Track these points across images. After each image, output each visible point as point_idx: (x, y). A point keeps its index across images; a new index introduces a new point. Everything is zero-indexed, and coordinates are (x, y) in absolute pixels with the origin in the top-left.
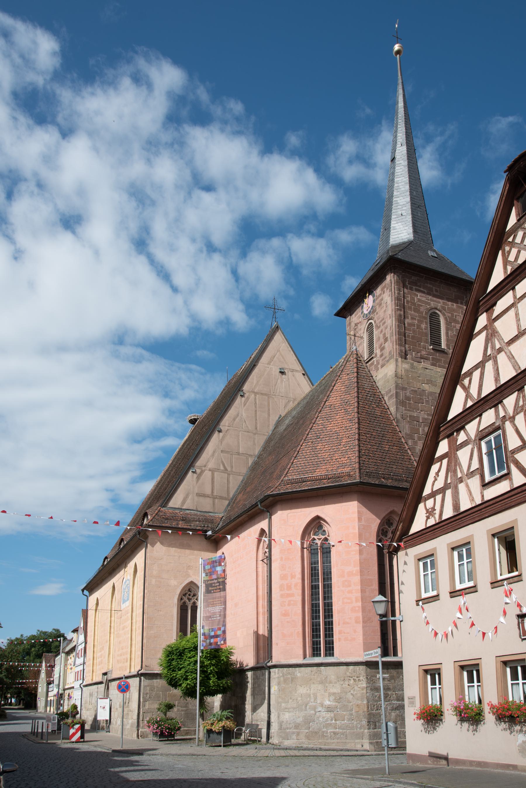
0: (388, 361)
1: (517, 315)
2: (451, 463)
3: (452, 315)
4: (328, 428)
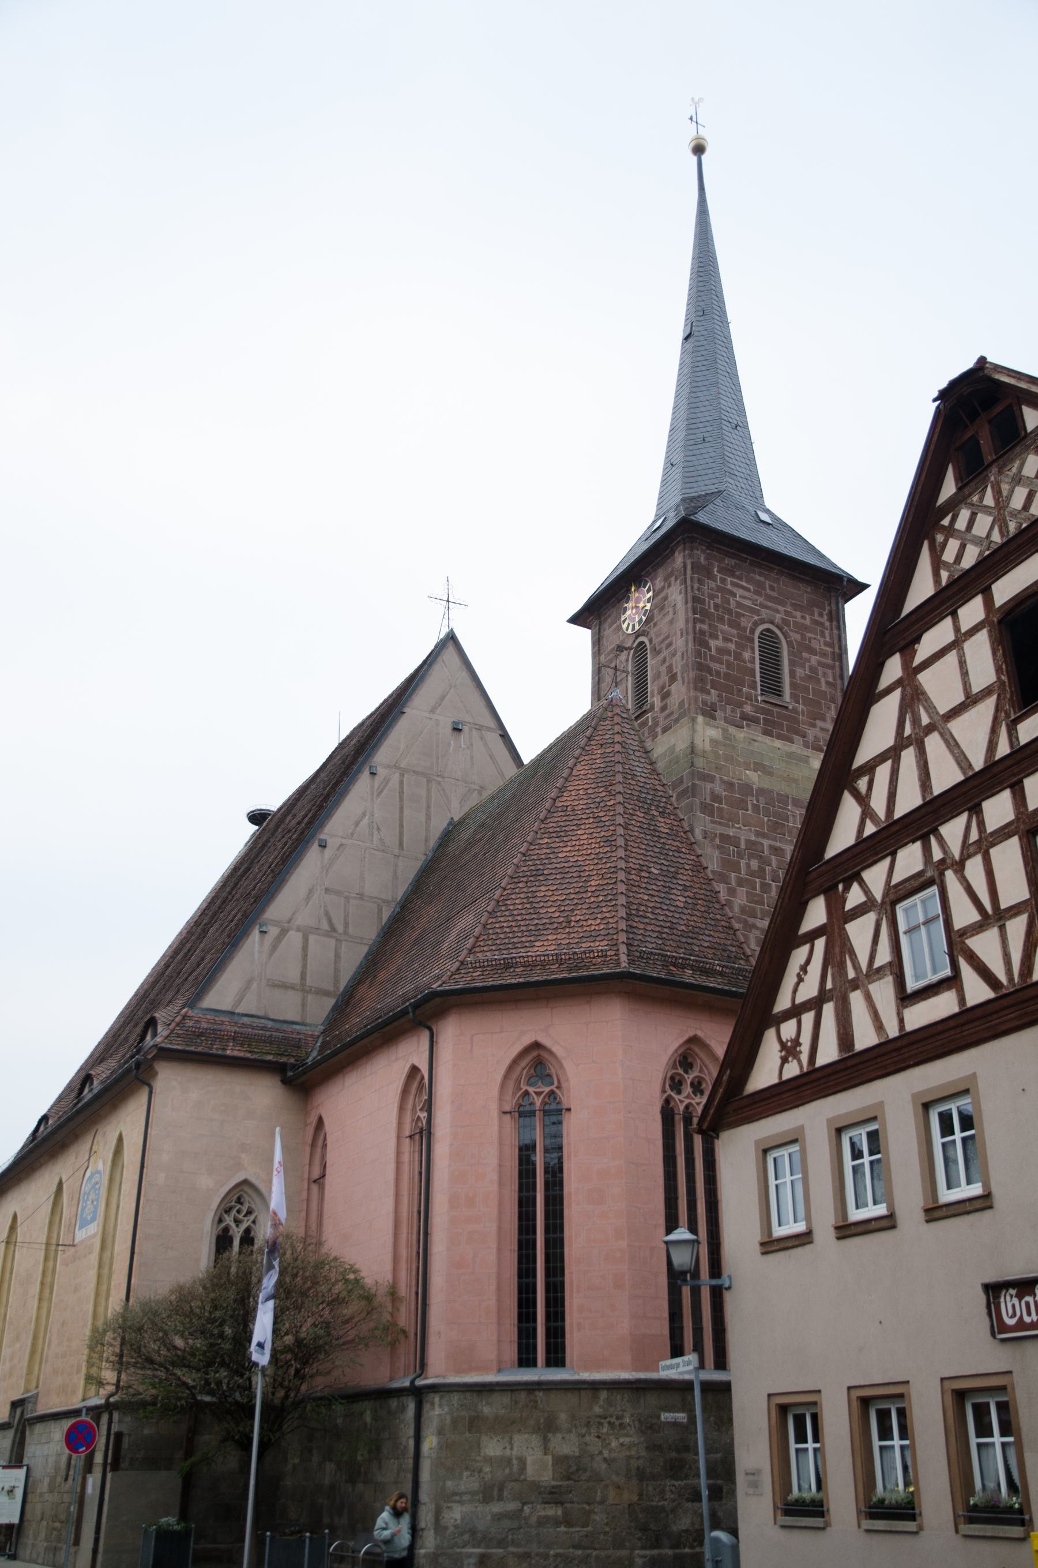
0: (677, 721)
1: (962, 663)
2: (833, 947)
3: (803, 637)
4: (560, 855)
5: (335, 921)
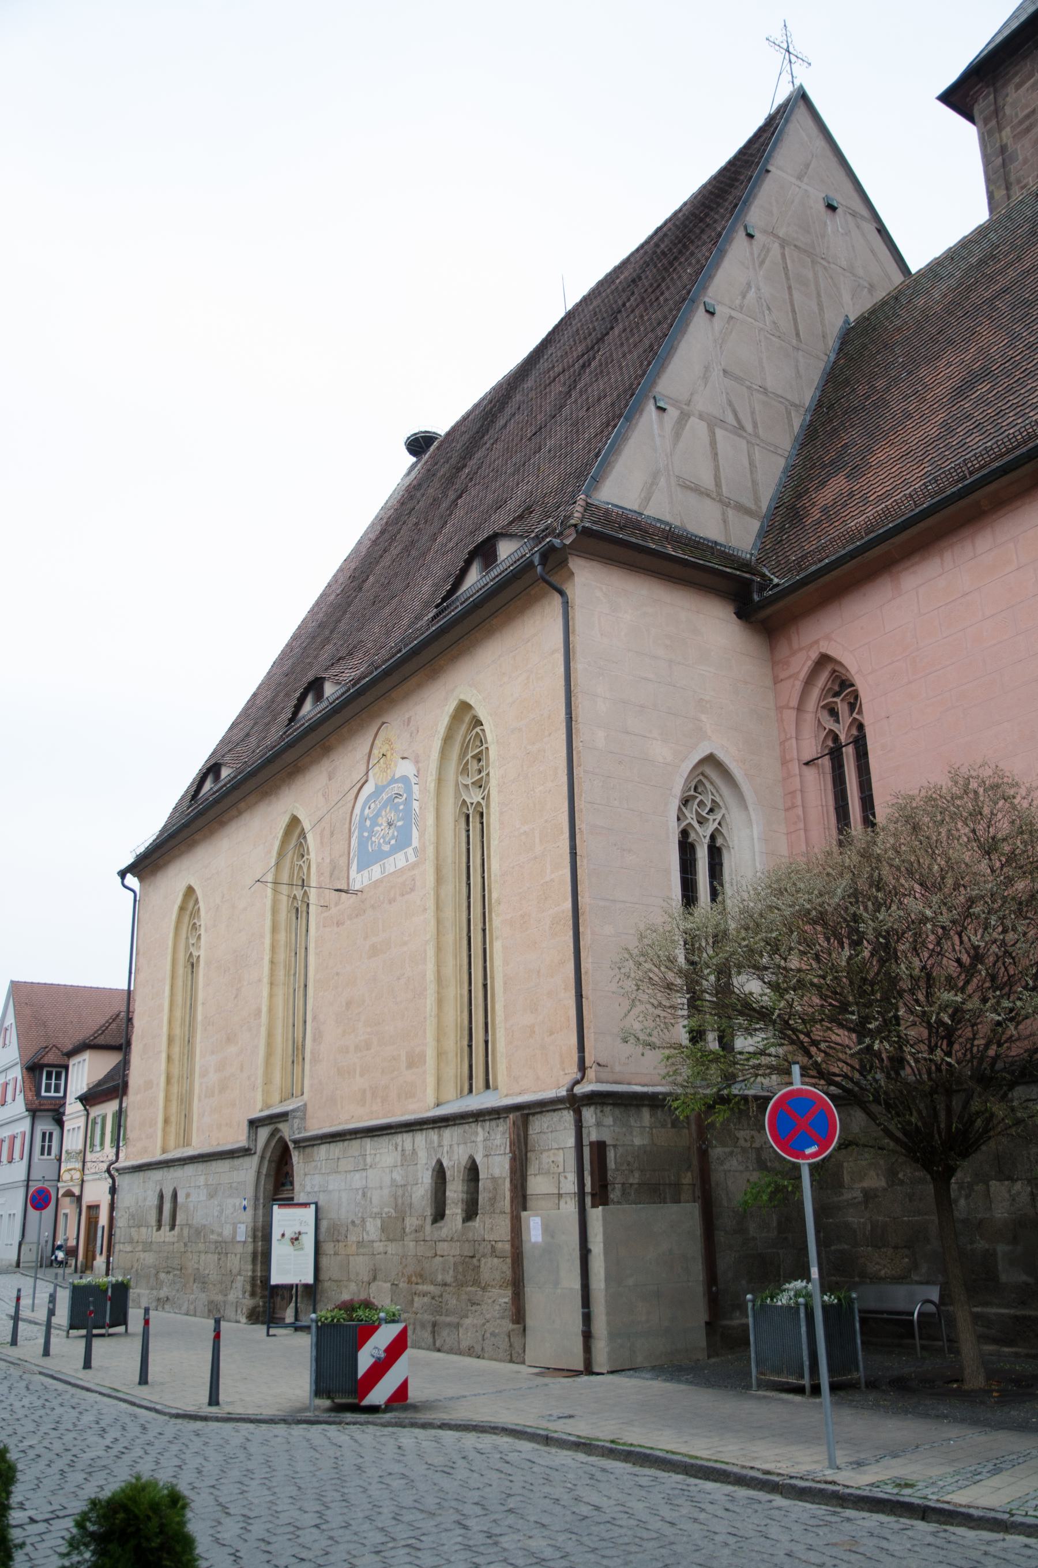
5: (741, 416)
